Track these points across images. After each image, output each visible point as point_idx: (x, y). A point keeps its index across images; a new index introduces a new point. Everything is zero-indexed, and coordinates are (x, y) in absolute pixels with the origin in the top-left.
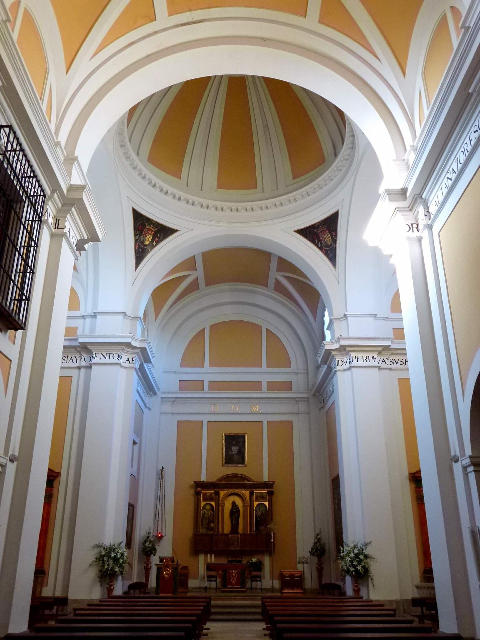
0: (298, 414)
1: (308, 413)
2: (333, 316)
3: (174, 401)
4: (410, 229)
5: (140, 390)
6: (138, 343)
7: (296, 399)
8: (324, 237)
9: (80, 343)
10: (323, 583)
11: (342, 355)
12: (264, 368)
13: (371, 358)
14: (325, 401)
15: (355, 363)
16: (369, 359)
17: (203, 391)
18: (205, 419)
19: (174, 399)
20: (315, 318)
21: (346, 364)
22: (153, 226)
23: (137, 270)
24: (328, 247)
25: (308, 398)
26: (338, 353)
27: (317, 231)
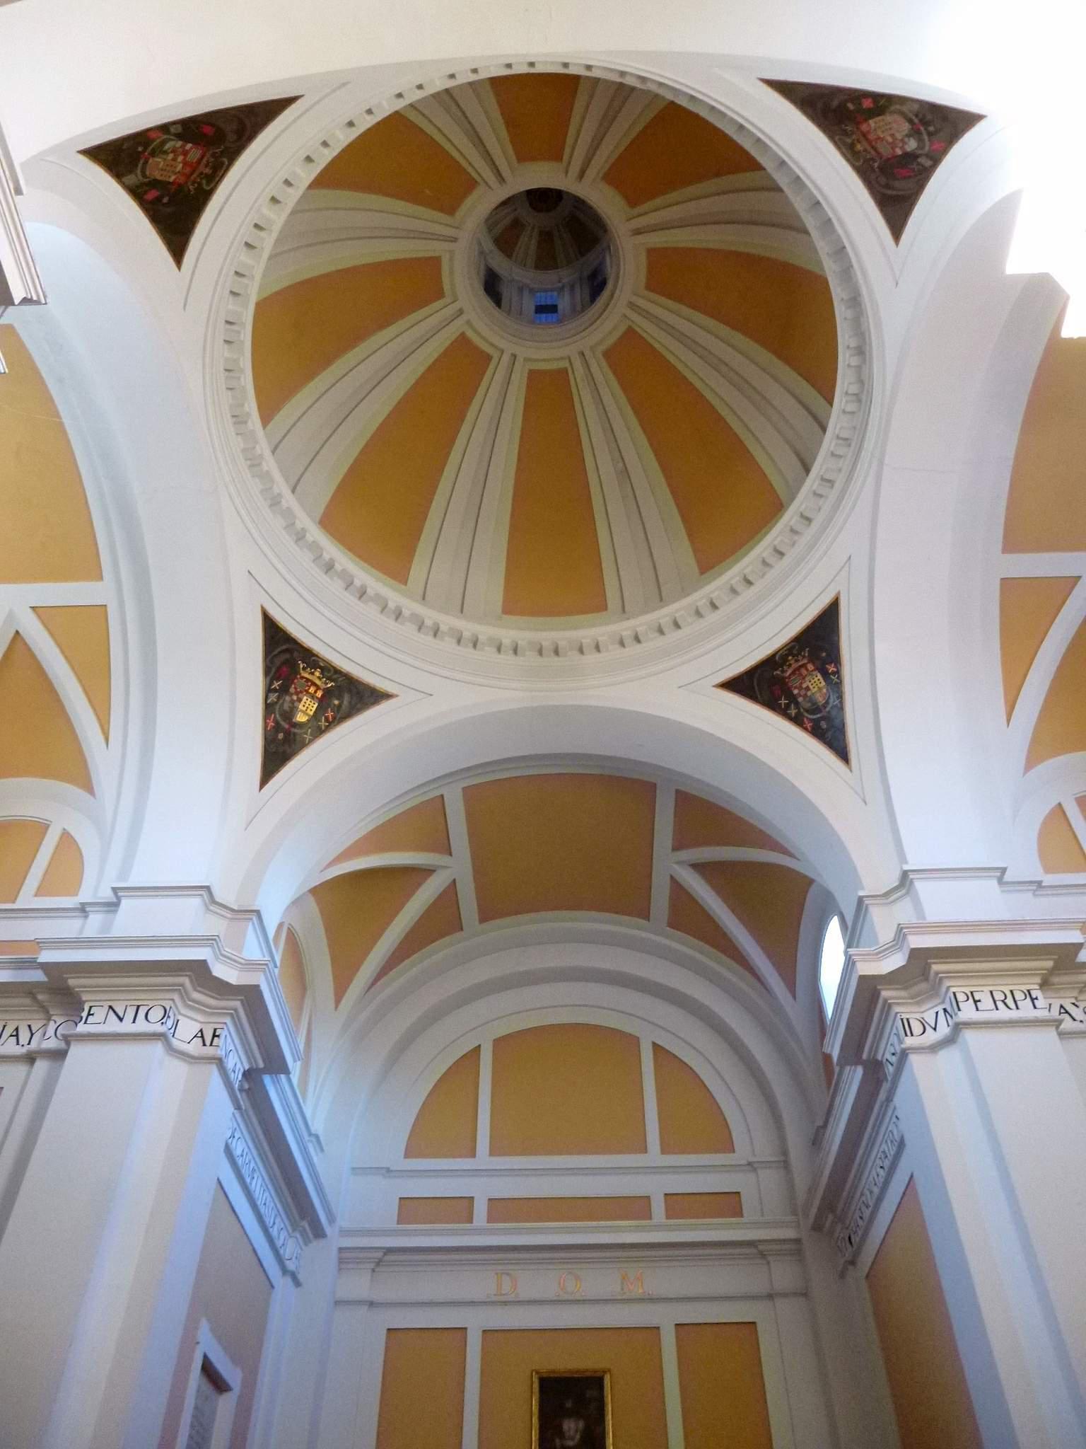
0: (770, 1297)
1: (805, 1294)
2: (863, 888)
3: (379, 1263)
5: (239, 1148)
6: (236, 973)
7: (761, 1247)
8: (804, 686)
9: (45, 967)
11: (918, 999)
12: (654, 1154)
13: (1019, 996)
14: (855, 1239)
15: (967, 1012)
16: (1015, 1002)
17: (468, 1226)
18: (475, 1322)
19: (379, 1254)
21: (935, 1029)
22: (322, 673)
23: (267, 787)
25: (798, 1241)
26: (903, 993)
27: (783, 671)
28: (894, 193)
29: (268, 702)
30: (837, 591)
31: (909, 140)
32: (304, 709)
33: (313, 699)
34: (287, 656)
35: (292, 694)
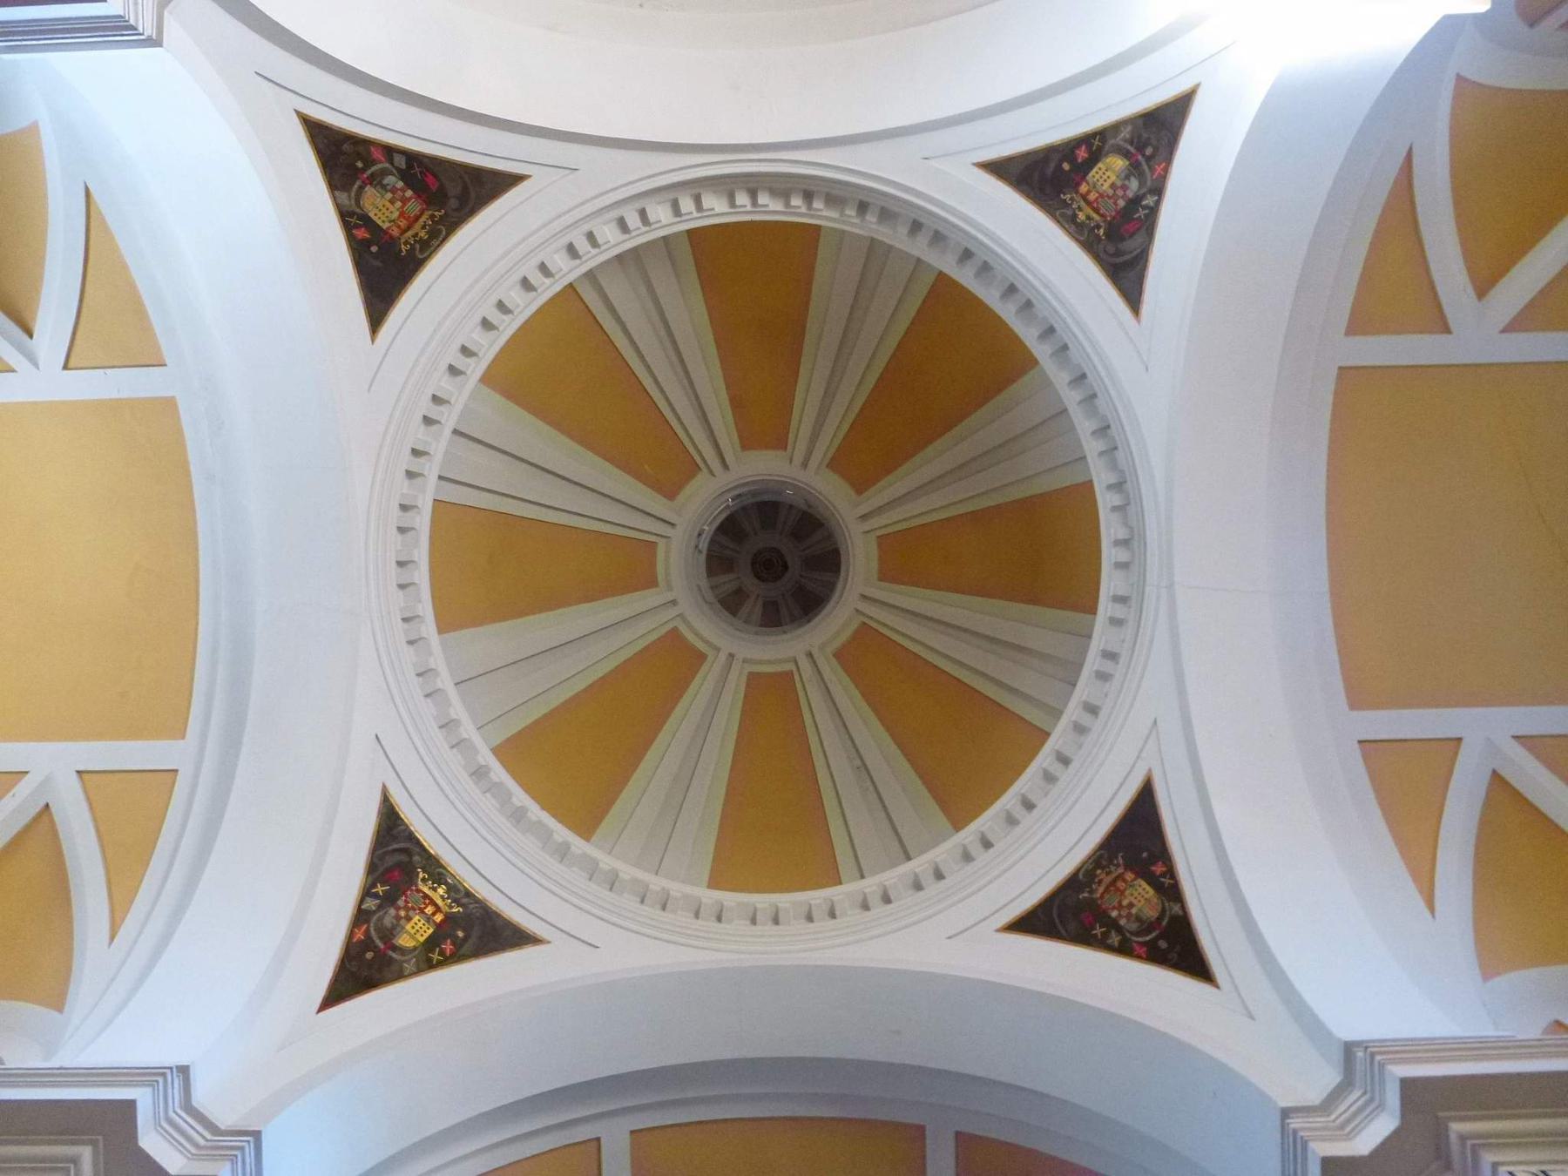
8: (1125, 903)
10: (395, 154)
22: (448, 892)
24: (1154, 929)
27: (1091, 892)
29: (363, 907)
31: (1134, 922)
32: (413, 931)
33: (428, 922)
34: (403, 858)
35: (398, 908)
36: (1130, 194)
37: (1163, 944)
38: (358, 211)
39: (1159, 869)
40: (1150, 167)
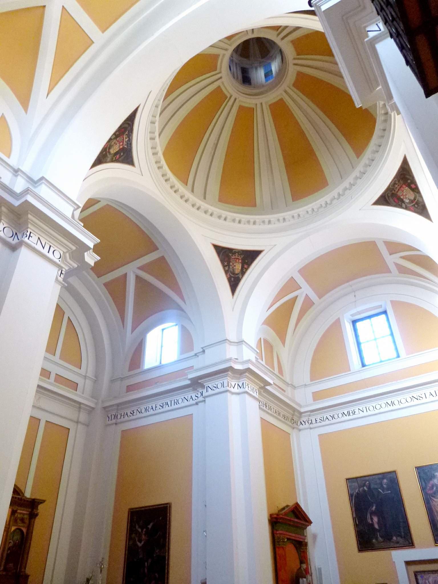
1: (87, 425)
4: (12, 237)
8: (235, 264)
20: (132, 331)
21: (234, 388)
26: (232, 375)
27: (232, 256)
28: (387, 199)
30: (264, 249)
34: (390, 198)
36: (405, 200)
37: (232, 279)
38: (416, 193)
39: (246, 266)
40: (412, 206)
